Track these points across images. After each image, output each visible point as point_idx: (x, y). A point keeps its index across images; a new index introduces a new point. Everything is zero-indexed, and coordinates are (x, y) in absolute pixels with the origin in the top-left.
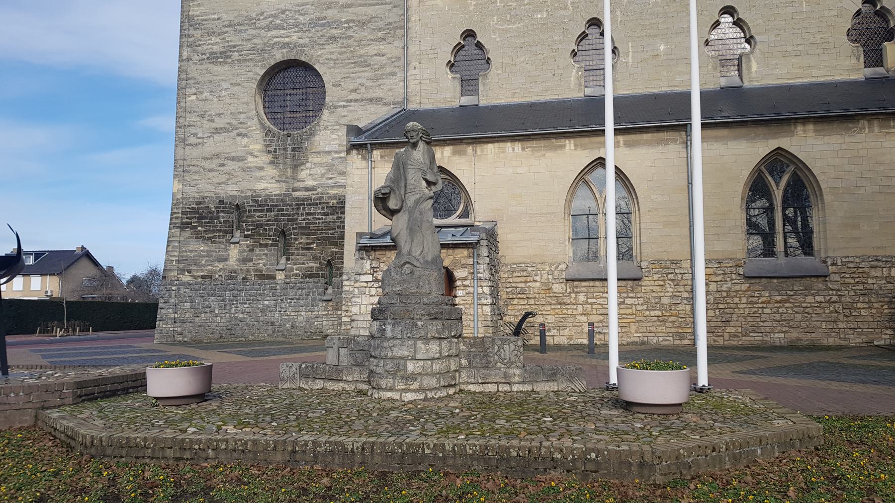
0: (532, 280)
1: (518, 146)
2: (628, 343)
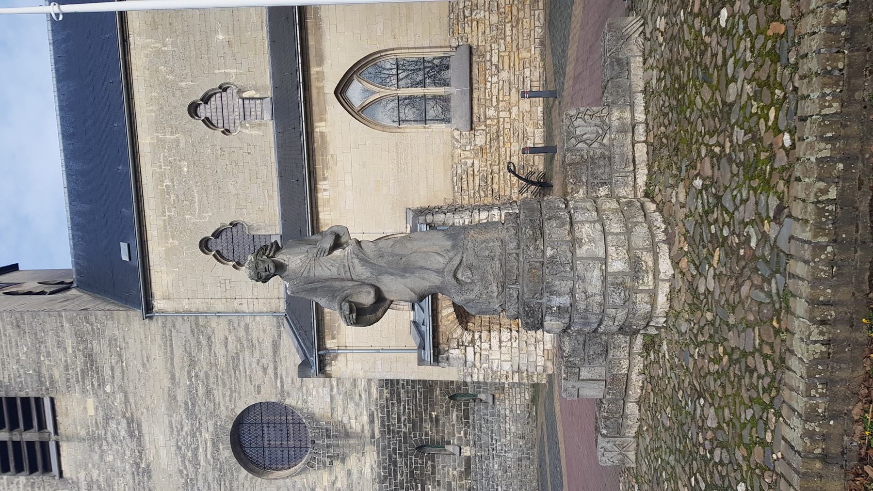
1: (322, 185)
2: (542, 60)
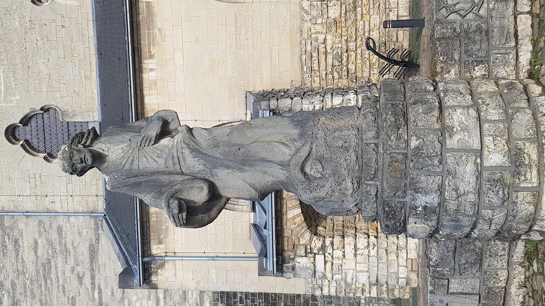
0: (324, 45)
1: (147, 64)
